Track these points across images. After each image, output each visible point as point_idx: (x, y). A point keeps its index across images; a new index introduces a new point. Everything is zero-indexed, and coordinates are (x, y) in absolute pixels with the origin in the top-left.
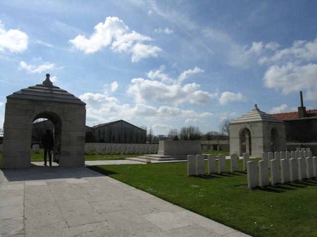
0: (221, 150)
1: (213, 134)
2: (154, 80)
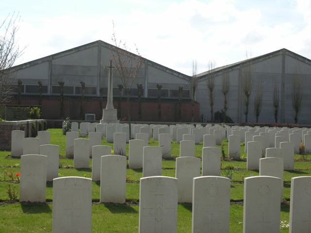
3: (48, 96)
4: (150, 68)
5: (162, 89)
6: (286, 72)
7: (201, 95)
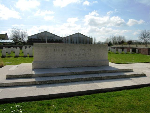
0: (139, 52)
1: (134, 41)
2: (92, 15)
3: (36, 41)
4: (55, 36)
5: (106, 30)
6: (3, 47)
7: (63, 40)
